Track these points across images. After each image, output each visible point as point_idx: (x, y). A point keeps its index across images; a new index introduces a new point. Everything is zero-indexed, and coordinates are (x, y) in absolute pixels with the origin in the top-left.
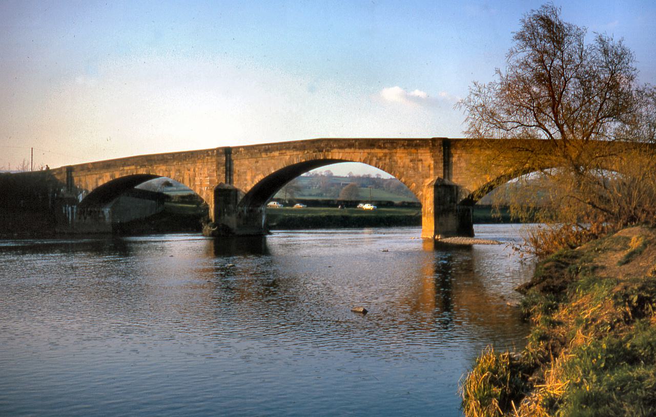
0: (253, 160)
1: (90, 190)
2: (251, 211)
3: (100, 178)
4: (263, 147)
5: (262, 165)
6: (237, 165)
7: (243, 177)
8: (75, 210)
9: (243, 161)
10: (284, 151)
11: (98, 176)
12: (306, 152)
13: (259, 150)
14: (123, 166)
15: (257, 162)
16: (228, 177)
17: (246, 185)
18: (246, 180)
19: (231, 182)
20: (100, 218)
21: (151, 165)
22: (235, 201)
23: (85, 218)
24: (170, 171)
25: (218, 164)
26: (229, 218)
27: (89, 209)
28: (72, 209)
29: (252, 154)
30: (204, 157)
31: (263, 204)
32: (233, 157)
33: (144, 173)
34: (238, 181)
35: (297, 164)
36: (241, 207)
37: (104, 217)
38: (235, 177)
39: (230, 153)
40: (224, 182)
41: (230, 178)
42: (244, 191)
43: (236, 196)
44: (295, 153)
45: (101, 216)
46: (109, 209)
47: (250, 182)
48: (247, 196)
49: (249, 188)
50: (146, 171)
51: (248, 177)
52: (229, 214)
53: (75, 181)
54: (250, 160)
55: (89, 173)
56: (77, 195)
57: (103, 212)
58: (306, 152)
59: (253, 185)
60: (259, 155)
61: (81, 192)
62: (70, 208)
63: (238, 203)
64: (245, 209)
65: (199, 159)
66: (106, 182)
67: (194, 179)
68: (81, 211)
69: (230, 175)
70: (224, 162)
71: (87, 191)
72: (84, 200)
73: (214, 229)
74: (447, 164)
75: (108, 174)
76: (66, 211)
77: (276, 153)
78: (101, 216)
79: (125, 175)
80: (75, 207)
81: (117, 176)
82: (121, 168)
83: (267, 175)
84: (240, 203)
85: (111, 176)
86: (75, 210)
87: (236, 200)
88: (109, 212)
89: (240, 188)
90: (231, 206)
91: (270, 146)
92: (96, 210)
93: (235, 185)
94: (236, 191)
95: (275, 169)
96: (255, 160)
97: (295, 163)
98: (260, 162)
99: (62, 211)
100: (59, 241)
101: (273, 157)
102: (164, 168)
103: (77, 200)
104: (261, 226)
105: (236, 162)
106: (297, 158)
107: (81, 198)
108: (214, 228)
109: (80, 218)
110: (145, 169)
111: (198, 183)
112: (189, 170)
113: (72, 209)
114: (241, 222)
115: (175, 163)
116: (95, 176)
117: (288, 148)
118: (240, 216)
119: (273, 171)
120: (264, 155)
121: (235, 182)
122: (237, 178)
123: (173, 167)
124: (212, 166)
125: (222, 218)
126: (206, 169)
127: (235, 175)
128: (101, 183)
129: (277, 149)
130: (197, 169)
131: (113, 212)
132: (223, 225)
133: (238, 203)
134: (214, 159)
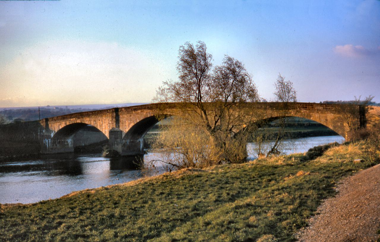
0: (129, 115)
1: (56, 131)
2: (132, 142)
3: (60, 125)
4: (133, 108)
5: (133, 118)
6: (121, 118)
7: (124, 124)
8: (50, 142)
9: (124, 115)
10: (143, 110)
11: (59, 123)
12: (153, 110)
13: (132, 110)
14: (70, 118)
15: (131, 116)
16: (117, 124)
17: (126, 128)
18: (126, 126)
19: (119, 127)
20: (66, 145)
21: (82, 118)
22: (120, 137)
23: (56, 145)
24: (91, 121)
25: (112, 117)
26: (118, 147)
27: (58, 141)
28: (48, 141)
29: (128, 112)
30: (106, 113)
31: (141, 137)
32: (120, 113)
33: (80, 122)
34: (122, 126)
35: (150, 117)
36: (125, 140)
37: (68, 144)
38: (121, 124)
39: (118, 111)
40: (115, 127)
41: (118, 126)
42: (125, 132)
43: (121, 134)
44: (148, 111)
45: (66, 144)
46: (71, 140)
47: (128, 127)
48: (127, 134)
49: (127, 130)
50: (80, 121)
51: (127, 124)
52: (117, 144)
53: (50, 126)
54: (127, 115)
55: (55, 122)
56: (51, 134)
57: (67, 142)
58: (153, 110)
59: (129, 129)
60: (131, 112)
61: (52, 132)
62: (47, 141)
63: (123, 138)
64: (128, 141)
65: (104, 115)
66: (63, 127)
67: (102, 125)
68: (53, 142)
69: (118, 123)
70: (115, 116)
71: (55, 132)
72: (55, 136)
73: (107, 153)
74: (117, 121)
75: (64, 123)
76: (45, 142)
77: (139, 111)
78: (66, 144)
79: (71, 123)
80: (50, 140)
81: (68, 124)
82: (69, 119)
83: (136, 123)
84: (124, 138)
85: (65, 124)
86: (50, 142)
87: (121, 137)
88: (71, 141)
89: (123, 130)
90: (119, 140)
91: (136, 107)
92: (63, 140)
93: (121, 129)
94: (121, 132)
95: (139, 120)
96: (130, 115)
97: (149, 116)
98: (132, 116)
99: (43, 142)
100: (17, 163)
101: (138, 113)
102: (88, 119)
103: (51, 136)
104: (140, 150)
105: (121, 116)
106: (148, 114)
107: (52, 135)
108: (107, 152)
109: (53, 146)
110: (80, 120)
111: (104, 127)
112: (100, 120)
113: (48, 141)
114: (125, 149)
115: (93, 117)
116: (58, 123)
117: (145, 108)
118: (124, 145)
119: (138, 121)
120: (134, 112)
121: (121, 127)
122: (122, 124)
123: (92, 119)
124: (110, 118)
125: (114, 147)
126: (107, 120)
127: (120, 123)
128: (61, 128)
129: (140, 109)
130: (103, 120)
131: (75, 141)
132: (114, 150)
133: (123, 138)
134: (110, 115)
